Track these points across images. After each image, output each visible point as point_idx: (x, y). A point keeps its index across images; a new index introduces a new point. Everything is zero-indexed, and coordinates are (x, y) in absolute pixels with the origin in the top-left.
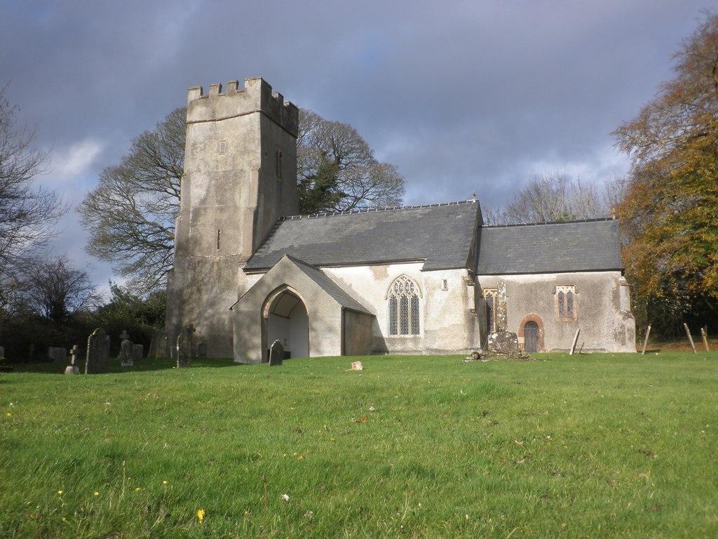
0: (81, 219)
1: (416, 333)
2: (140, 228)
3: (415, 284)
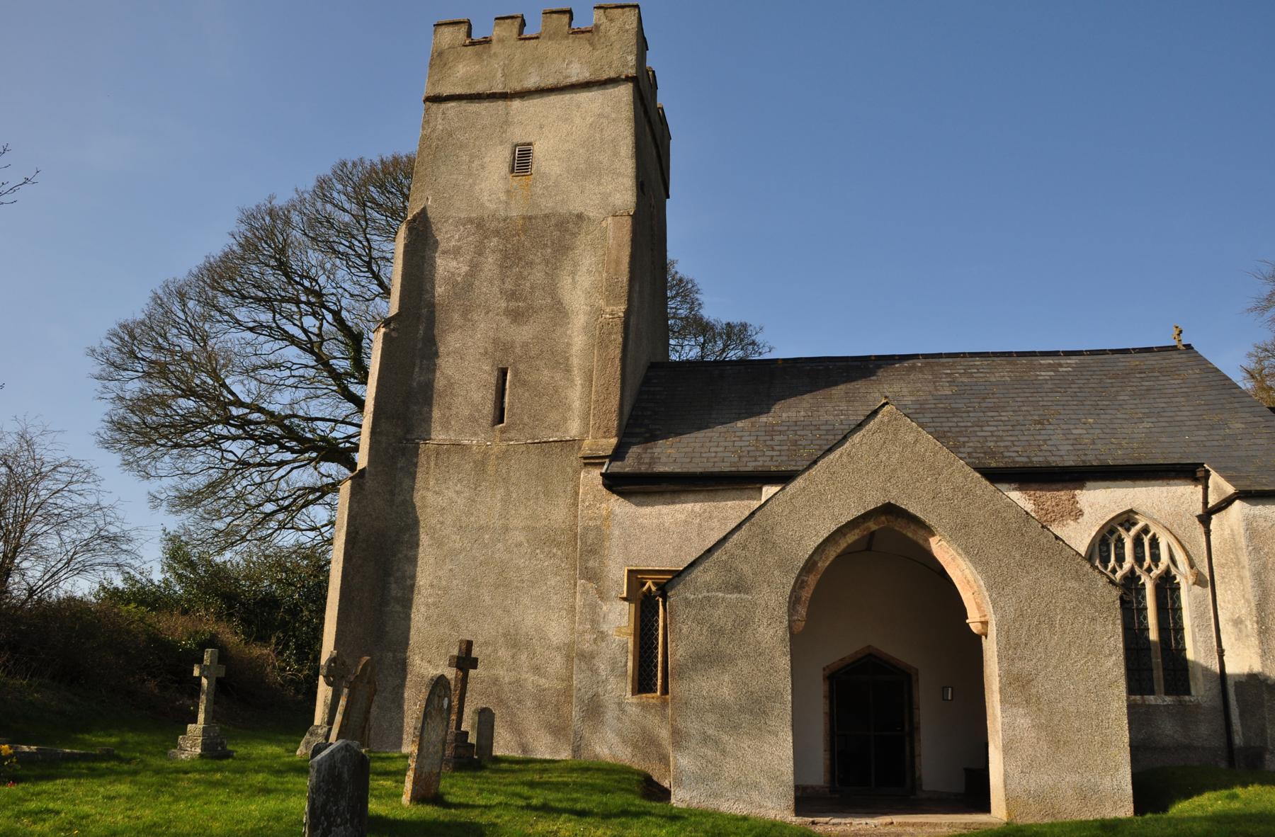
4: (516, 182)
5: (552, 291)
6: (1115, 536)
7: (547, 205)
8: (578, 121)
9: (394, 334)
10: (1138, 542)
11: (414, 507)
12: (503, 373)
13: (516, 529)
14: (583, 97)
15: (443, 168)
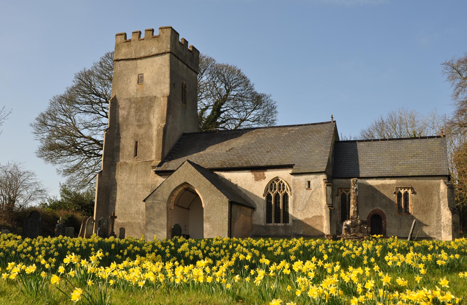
0: (34, 131)
1: (286, 223)
2: (78, 140)
3: (286, 184)
4: (139, 87)
5: (148, 119)
6: (274, 183)
7: (147, 93)
8: (155, 66)
9: (108, 133)
10: (280, 185)
11: (115, 179)
12: (137, 142)
13: (139, 184)
14: (157, 58)
15: (120, 83)
